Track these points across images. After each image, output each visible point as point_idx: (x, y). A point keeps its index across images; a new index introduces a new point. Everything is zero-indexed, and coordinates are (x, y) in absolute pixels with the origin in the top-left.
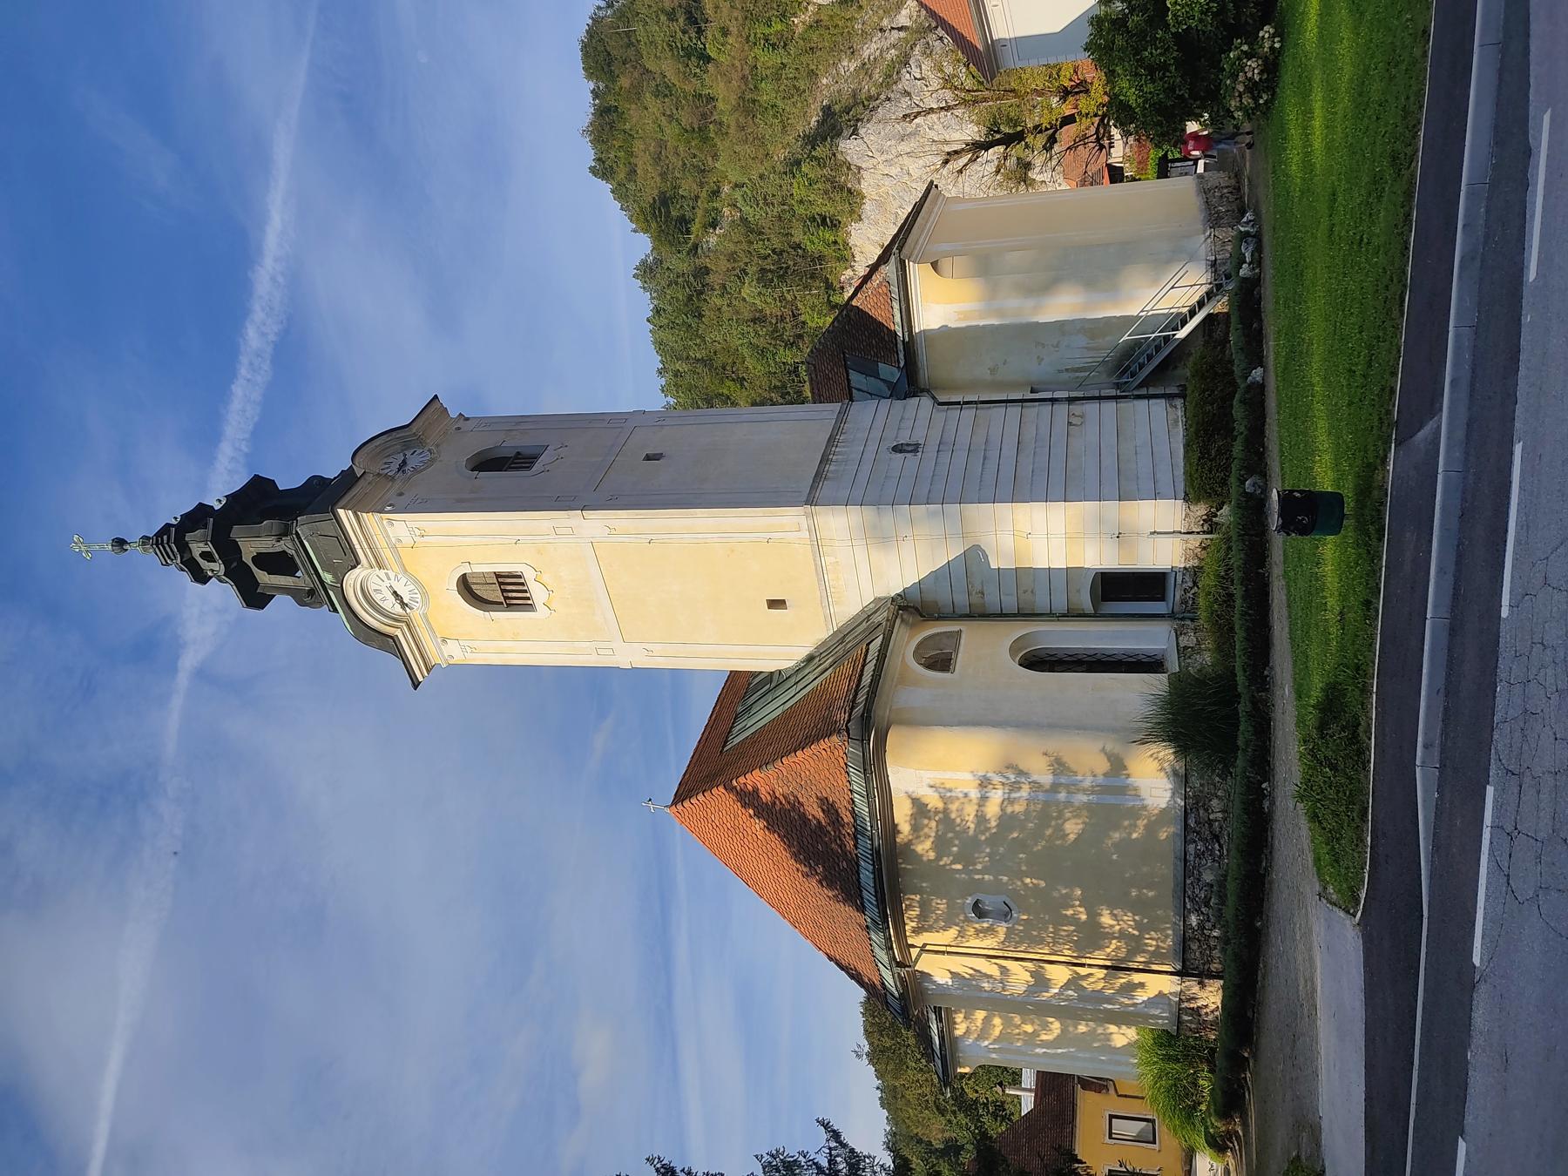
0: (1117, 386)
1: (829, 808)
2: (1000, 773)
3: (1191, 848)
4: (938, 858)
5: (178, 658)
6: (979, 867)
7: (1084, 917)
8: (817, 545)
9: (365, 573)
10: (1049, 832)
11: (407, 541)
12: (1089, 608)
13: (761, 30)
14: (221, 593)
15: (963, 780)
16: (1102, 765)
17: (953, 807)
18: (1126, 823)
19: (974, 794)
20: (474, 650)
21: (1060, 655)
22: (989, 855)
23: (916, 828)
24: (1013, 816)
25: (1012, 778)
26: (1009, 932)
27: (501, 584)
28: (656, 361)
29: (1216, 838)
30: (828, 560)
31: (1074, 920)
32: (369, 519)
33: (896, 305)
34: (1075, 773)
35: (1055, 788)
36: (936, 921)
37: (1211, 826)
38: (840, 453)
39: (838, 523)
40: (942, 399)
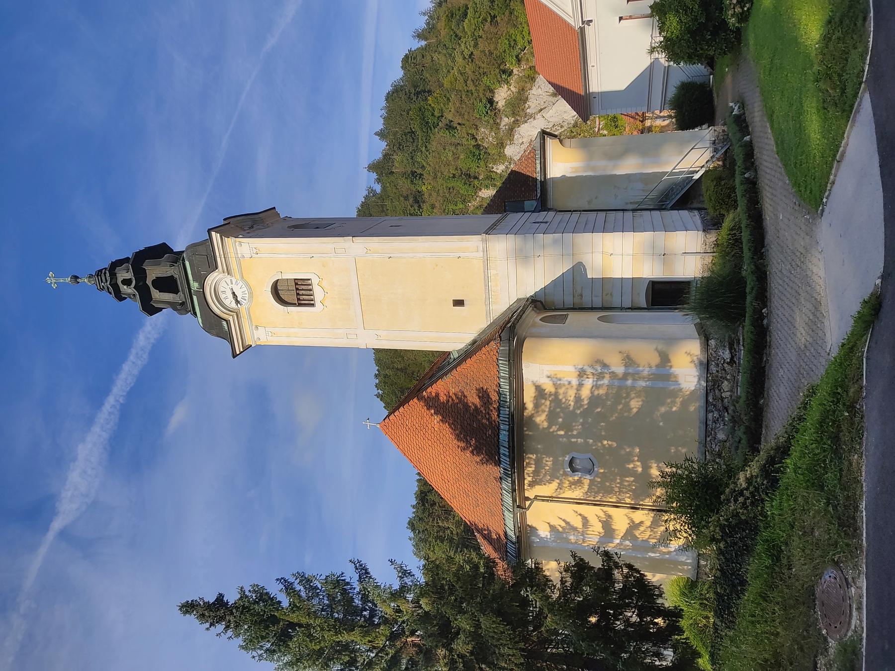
1: (483, 395)
2: (592, 366)
3: (710, 416)
4: (549, 427)
5: (52, 521)
6: (575, 433)
7: (640, 470)
8: (487, 261)
9: (221, 276)
10: (620, 407)
11: (247, 255)
12: (644, 304)
13: (451, 207)
15: (567, 371)
16: (655, 360)
17: (561, 391)
18: (669, 400)
19: (575, 382)
20: (273, 334)
22: (582, 424)
23: (537, 406)
24: (599, 396)
25: (599, 369)
26: (592, 483)
28: (375, 369)
30: (492, 272)
31: (633, 473)
32: (229, 241)
33: (538, 162)
34: (638, 366)
35: (625, 376)
36: (545, 475)
37: (722, 401)
39: (501, 246)
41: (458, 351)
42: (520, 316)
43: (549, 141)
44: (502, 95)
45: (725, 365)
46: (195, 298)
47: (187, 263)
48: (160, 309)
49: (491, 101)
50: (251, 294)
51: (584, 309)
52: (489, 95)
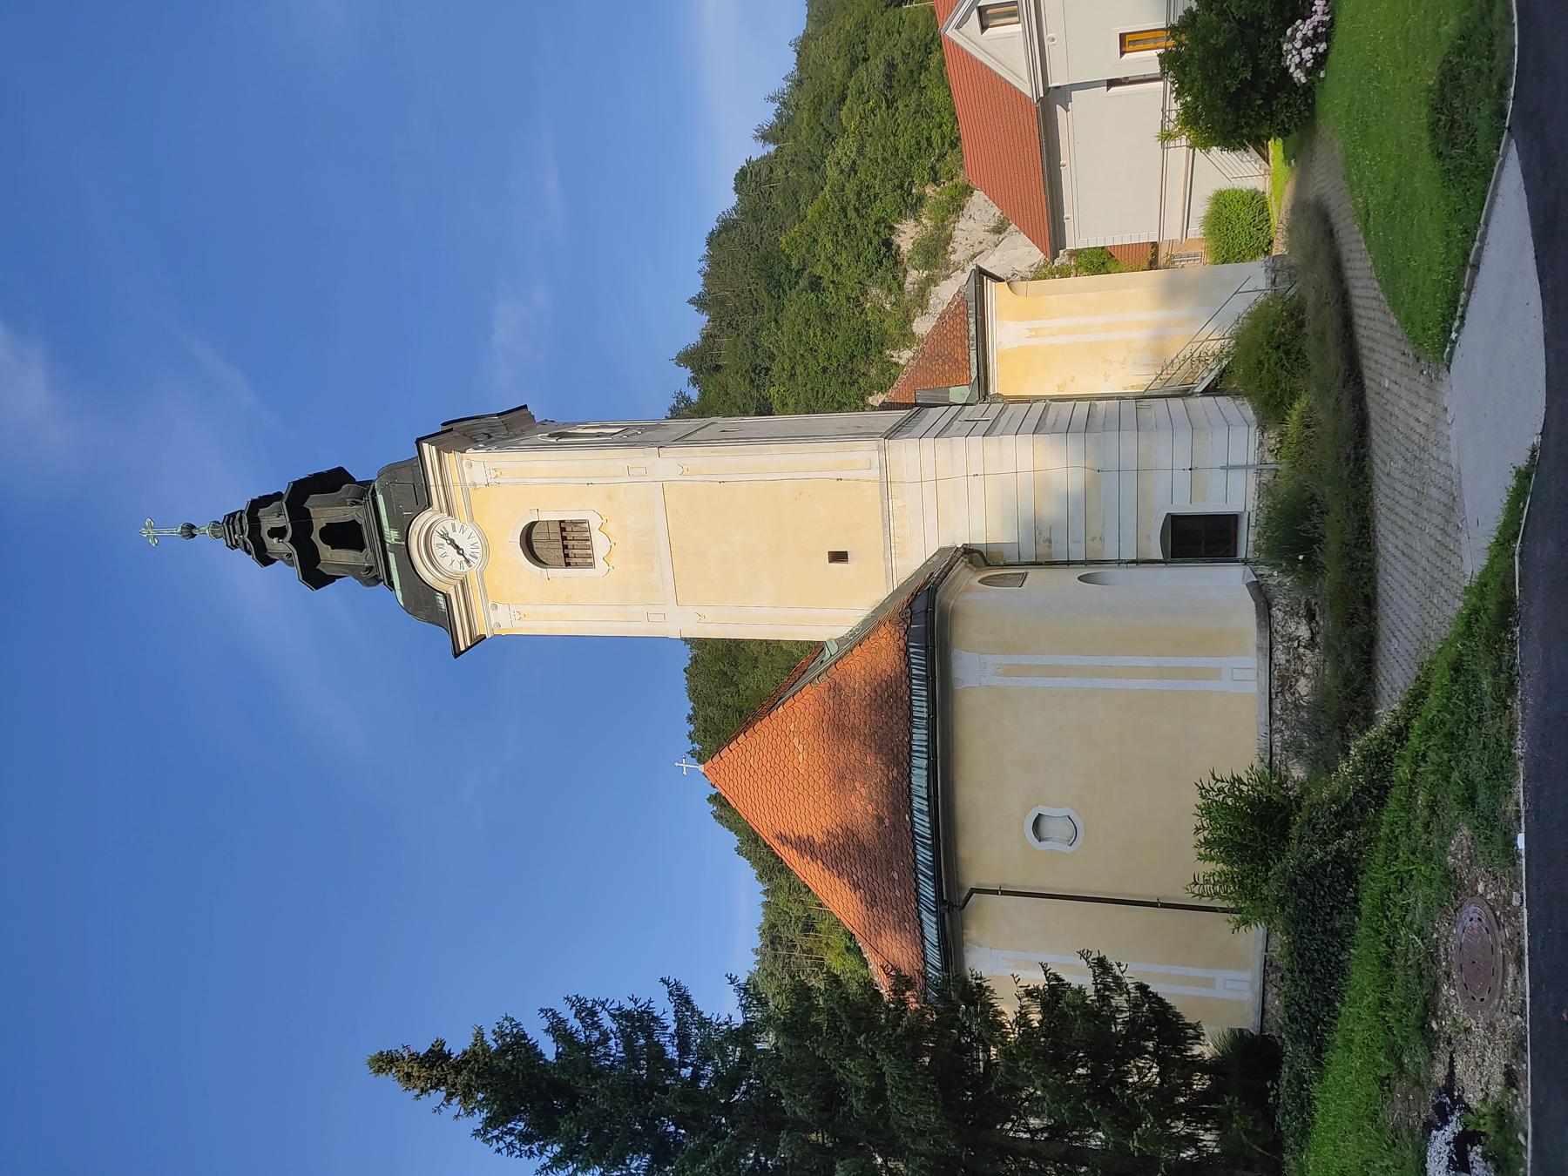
8: (886, 484)
14: (286, 574)
28: (687, 707)
30: (895, 504)
32: (450, 458)
41: (839, 642)
42: (945, 573)
43: (990, 285)
44: (907, 236)
45: (1301, 650)
46: (391, 557)
47: (380, 498)
48: (332, 579)
49: (888, 243)
50: (486, 548)
51: (1055, 563)
52: (884, 233)
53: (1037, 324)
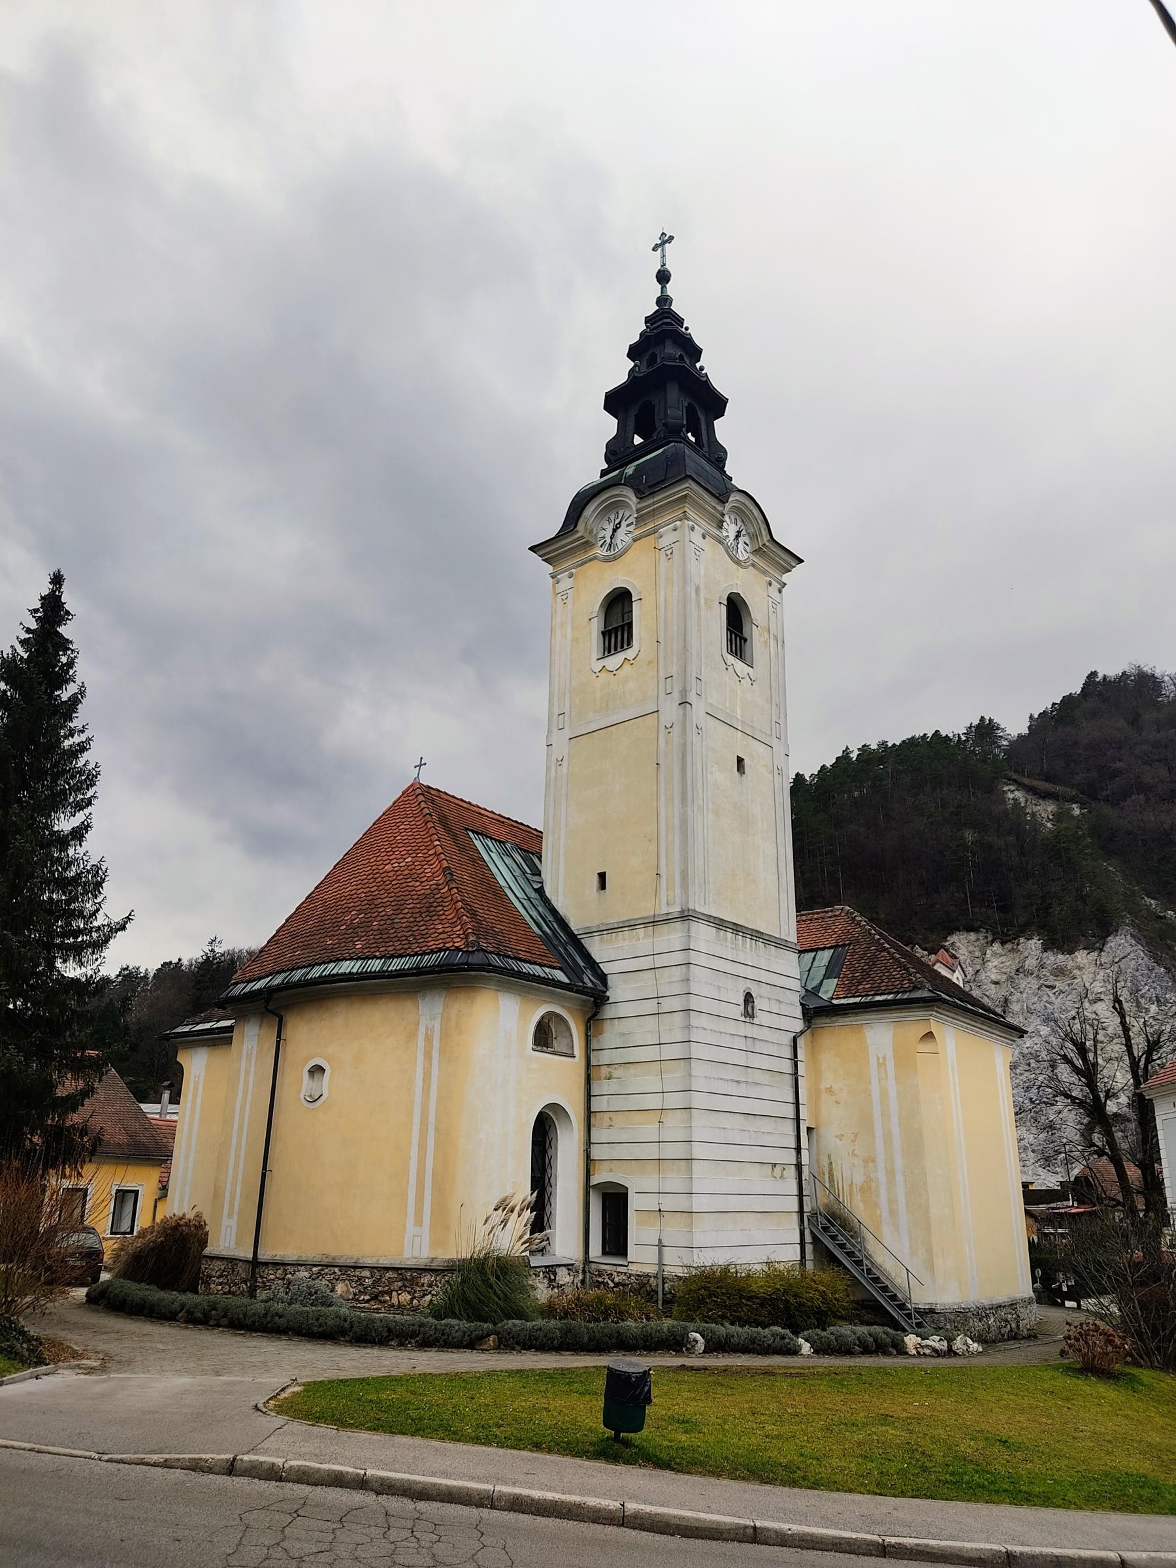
0: (814, 1214)
3: (367, 1273)
8: (653, 922)
11: (663, 542)
12: (595, 1180)
21: (550, 1152)
27: (622, 627)
29: (375, 1298)
30: (641, 932)
33: (890, 997)
38: (744, 943)
40: (801, 1042)
53: (890, 1064)
